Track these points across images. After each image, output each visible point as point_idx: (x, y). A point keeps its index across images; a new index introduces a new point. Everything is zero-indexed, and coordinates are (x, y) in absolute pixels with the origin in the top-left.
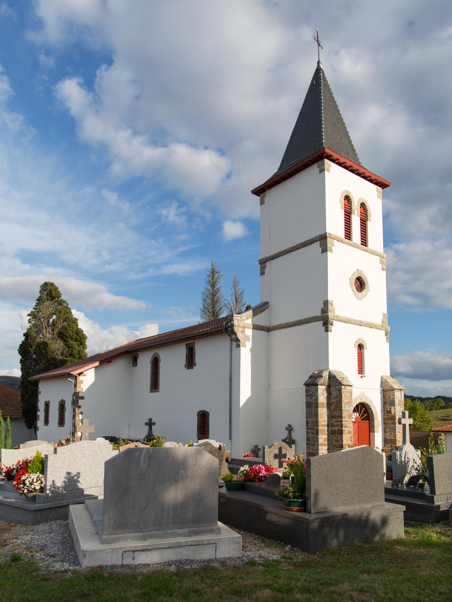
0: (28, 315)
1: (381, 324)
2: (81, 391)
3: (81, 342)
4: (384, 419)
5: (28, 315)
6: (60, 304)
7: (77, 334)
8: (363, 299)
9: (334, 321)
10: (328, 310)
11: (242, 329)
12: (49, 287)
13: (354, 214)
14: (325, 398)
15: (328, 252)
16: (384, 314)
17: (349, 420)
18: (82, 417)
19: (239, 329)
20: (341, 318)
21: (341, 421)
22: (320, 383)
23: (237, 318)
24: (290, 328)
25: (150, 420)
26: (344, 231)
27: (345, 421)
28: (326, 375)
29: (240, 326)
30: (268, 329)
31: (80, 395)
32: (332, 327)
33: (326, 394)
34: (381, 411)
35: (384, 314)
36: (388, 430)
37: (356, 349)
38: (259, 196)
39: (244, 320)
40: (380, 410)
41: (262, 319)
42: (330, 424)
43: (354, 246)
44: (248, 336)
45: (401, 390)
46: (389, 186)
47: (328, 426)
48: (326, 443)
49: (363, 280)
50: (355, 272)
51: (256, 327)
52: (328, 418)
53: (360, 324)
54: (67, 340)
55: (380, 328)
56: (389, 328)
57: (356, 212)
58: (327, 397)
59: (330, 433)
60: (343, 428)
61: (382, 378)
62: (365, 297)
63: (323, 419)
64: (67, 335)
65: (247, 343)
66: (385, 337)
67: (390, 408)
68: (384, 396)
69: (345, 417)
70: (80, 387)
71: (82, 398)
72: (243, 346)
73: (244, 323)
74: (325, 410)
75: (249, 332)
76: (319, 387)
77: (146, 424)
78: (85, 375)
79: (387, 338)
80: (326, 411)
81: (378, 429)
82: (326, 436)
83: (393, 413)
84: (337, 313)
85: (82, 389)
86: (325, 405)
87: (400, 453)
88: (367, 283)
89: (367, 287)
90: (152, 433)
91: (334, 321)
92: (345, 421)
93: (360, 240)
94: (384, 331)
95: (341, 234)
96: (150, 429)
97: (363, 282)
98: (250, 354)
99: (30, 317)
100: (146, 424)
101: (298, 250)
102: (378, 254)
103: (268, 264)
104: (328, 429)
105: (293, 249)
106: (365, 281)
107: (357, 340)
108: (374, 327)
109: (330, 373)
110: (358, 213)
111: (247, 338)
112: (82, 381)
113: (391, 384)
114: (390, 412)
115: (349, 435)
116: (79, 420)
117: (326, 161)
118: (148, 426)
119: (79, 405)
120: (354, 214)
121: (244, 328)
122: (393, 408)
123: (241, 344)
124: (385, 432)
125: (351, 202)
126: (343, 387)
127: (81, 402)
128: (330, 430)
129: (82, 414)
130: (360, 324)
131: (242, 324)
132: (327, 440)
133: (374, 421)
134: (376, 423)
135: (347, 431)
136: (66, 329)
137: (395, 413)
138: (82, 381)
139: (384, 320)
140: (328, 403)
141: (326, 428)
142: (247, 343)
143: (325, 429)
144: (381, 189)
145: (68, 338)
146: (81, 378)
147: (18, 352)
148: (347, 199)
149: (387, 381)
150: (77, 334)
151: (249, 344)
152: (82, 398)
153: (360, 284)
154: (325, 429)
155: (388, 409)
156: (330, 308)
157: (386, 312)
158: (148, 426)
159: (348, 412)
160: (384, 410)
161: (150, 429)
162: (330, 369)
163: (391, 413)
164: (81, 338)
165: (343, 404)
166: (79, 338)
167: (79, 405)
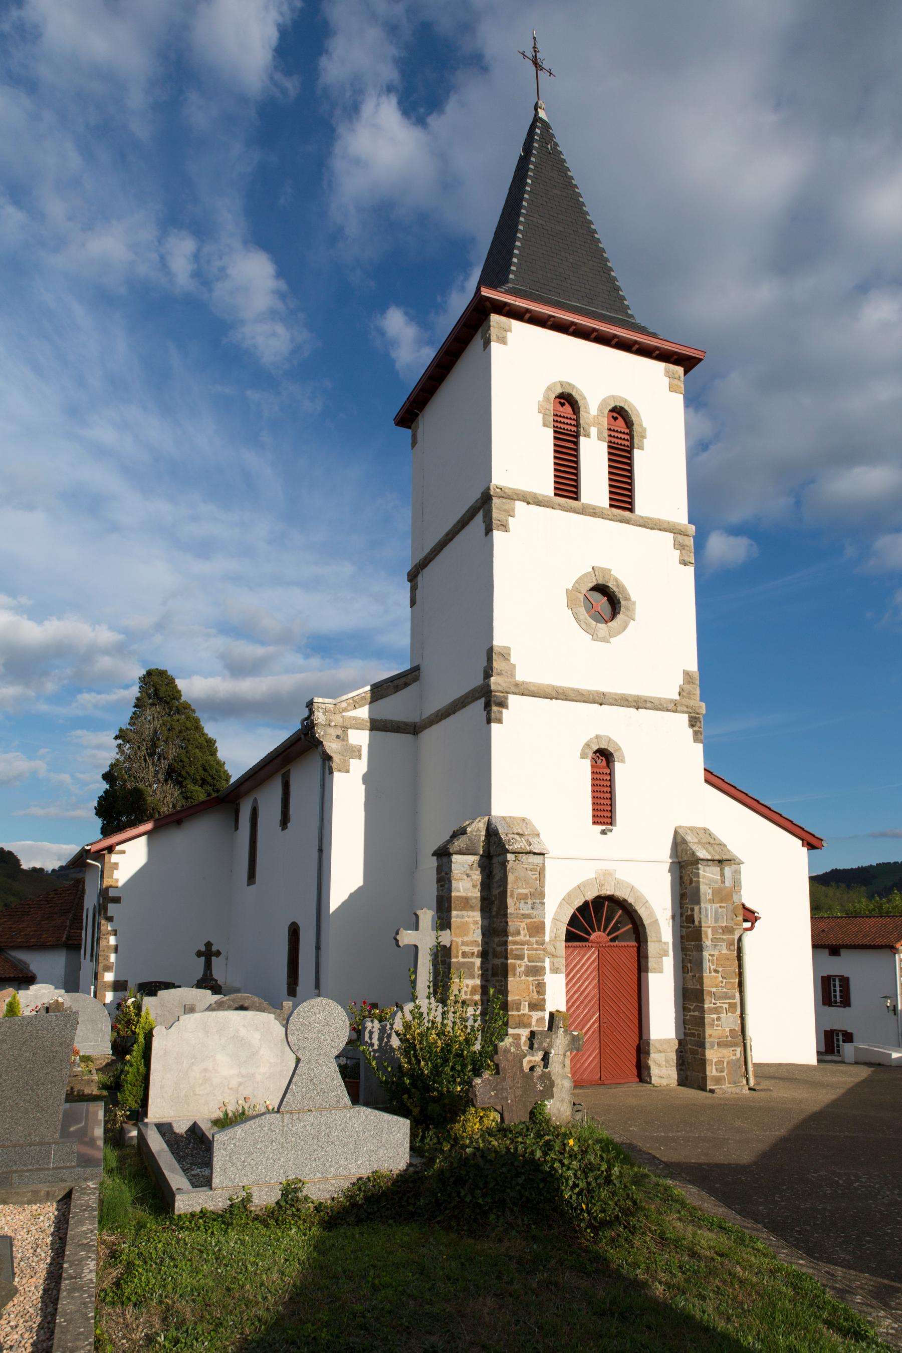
0: (116, 738)
1: (678, 698)
2: (114, 884)
3: (214, 785)
4: (682, 937)
5: (116, 738)
6: (178, 711)
7: (205, 770)
8: (612, 640)
9: (510, 697)
10: (492, 671)
11: (339, 732)
12: (155, 679)
13: (588, 435)
14: (474, 886)
15: (494, 531)
16: (687, 674)
17: (533, 940)
18: (117, 940)
19: (331, 731)
20: (533, 688)
21: (505, 943)
22: (457, 849)
23: (324, 706)
24: (443, 723)
25: (209, 945)
26: (607, 482)
27: (515, 943)
28: (478, 828)
29: (333, 724)
30: (414, 729)
31: (112, 893)
32: (504, 711)
33: (477, 876)
34: (673, 917)
35: (687, 674)
36: (689, 965)
37: (587, 763)
38: (409, 427)
39: (345, 710)
40: (669, 913)
41: (397, 707)
42: (491, 950)
43: (592, 512)
44: (355, 746)
45: (720, 861)
46: (700, 360)
47: (484, 955)
48: (477, 997)
49: (614, 592)
50: (585, 575)
51: (377, 726)
52: (483, 934)
53: (601, 699)
54: (184, 784)
55: (671, 706)
56: (703, 708)
57: (594, 431)
58: (482, 884)
59: (490, 972)
60: (509, 961)
61: (676, 832)
62: (620, 633)
63: (465, 939)
64: (183, 773)
65: (353, 762)
66: (691, 731)
67: (692, 910)
68: (681, 878)
69: (518, 933)
70: (111, 876)
71: (117, 900)
72: (339, 771)
73: (343, 717)
74: (476, 916)
75: (360, 738)
76: (455, 858)
77: (199, 954)
78: (123, 852)
79: (696, 733)
80: (479, 919)
81: (660, 964)
82: (478, 982)
83: (697, 923)
84: (520, 677)
85: (117, 880)
86: (478, 904)
87: (382, 1030)
88: (627, 599)
89: (627, 609)
90: (211, 975)
91: (510, 697)
92: (515, 943)
93: (607, 495)
94: (687, 716)
95: (545, 485)
96: (208, 966)
97: (616, 596)
98: (362, 788)
99: (120, 741)
100: (199, 954)
101: (458, 537)
102: (666, 526)
103: (420, 578)
104: (482, 963)
105: (450, 536)
106: (620, 596)
107: (591, 740)
108: (649, 705)
109: (489, 824)
110: (600, 432)
111: (356, 753)
112: (117, 864)
113: (694, 847)
114: (691, 919)
115: (531, 979)
116: (108, 947)
117: (495, 318)
118: (203, 959)
119: (109, 914)
120: (588, 435)
121: (345, 728)
122: (696, 908)
123: (334, 765)
124: (684, 972)
125: (579, 407)
126: (510, 857)
127: (112, 908)
128: (490, 966)
129: (115, 935)
130: (601, 699)
131: (337, 719)
132: (480, 991)
133: (647, 941)
134: (652, 948)
135: (523, 969)
136: (181, 761)
137: (700, 922)
138: (117, 864)
139: (687, 687)
140: (483, 899)
141: (478, 962)
142: (353, 762)
143: (473, 963)
144: (680, 370)
145: (185, 779)
146: (114, 858)
147: (94, 811)
148: (567, 400)
149: (684, 841)
150: (205, 770)
151: (359, 767)
152: (117, 900)
153: (606, 601)
154: (473, 963)
155: (689, 913)
156: (497, 664)
157: (693, 667)
158: (203, 959)
159: (528, 921)
160: (682, 915)
161: (208, 966)
162: (493, 813)
163: (693, 921)
164: (214, 779)
165: (510, 901)
166: (209, 779)
167: (109, 914)
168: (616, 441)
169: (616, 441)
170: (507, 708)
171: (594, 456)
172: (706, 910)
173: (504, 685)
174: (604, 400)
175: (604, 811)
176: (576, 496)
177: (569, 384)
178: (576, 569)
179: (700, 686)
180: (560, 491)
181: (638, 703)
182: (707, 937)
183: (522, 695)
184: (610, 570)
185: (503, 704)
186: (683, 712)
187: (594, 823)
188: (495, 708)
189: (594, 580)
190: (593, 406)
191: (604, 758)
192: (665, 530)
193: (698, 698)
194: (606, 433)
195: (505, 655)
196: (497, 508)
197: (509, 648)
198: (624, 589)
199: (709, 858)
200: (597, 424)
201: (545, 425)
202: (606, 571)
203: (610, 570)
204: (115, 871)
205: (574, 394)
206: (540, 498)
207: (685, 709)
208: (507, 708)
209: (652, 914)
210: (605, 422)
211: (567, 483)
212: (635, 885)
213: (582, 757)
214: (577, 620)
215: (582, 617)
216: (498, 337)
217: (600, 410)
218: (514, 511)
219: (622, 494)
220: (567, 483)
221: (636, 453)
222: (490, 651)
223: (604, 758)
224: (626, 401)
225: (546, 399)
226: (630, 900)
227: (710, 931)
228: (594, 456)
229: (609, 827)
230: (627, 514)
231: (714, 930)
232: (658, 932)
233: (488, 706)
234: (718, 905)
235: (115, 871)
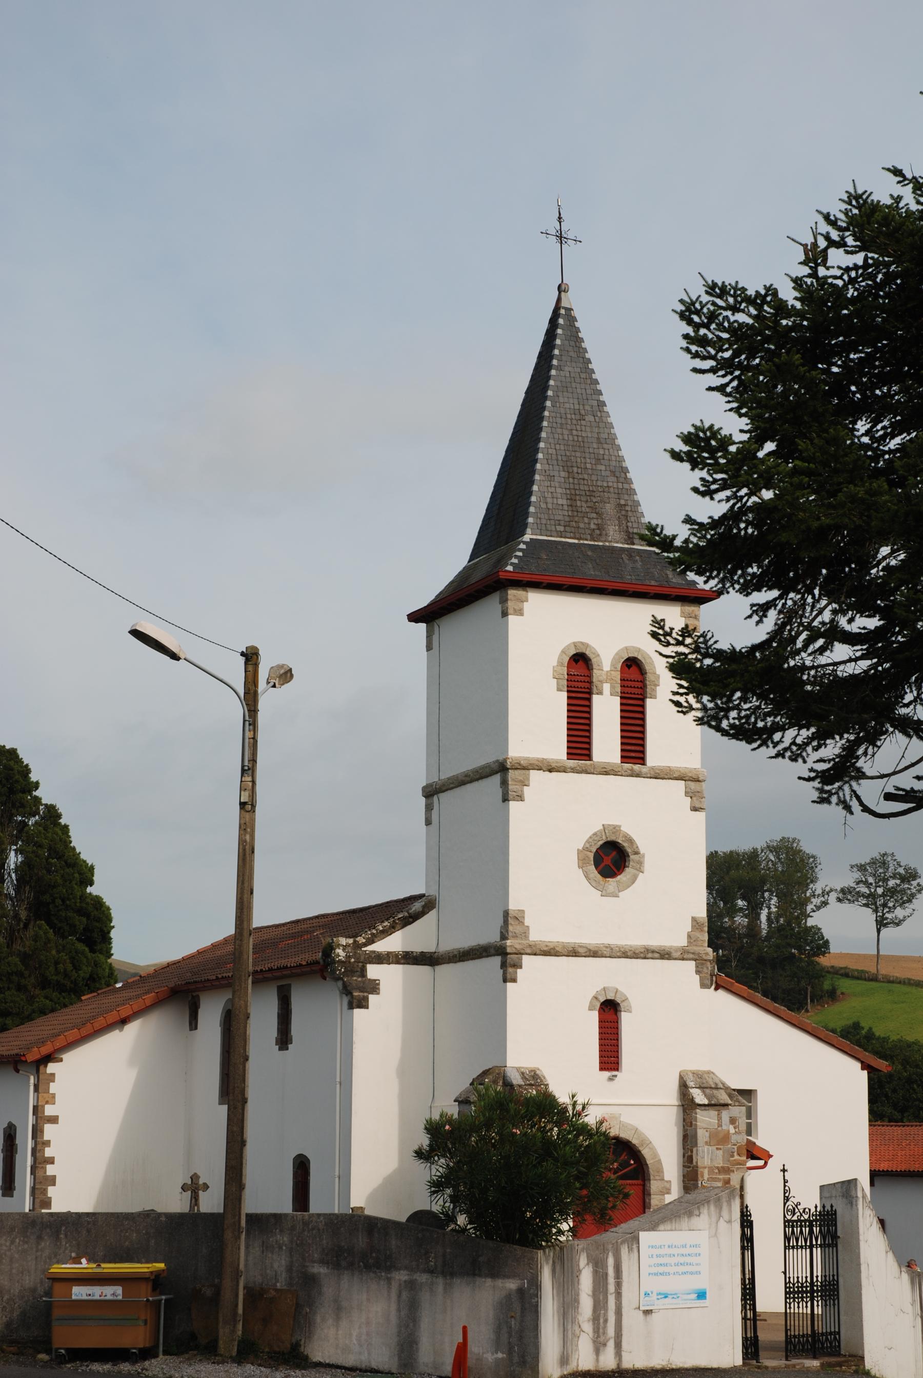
8: (621, 894)
13: (600, 693)
32: (519, 970)
37: (595, 1015)
43: (606, 771)
57: (606, 688)
95: (558, 750)
110: (612, 687)
122: (694, 1149)
153: (612, 858)
168: (576, 684)
169: (576, 684)
170: (521, 967)
171: (606, 711)
172: (703, 1152)
173: (518, 946)
174: (617, 654)
175: (610, 1058)
176: (642, 760)
177: (582, 643)
178: (585, 829)
179: (708, 932)
180: (626, 757)
181: (646, 953)
182: (702, 1176)
183: (535, 954)
184: (620, 826)
185: (518, 965)
186: (690, 959)
187: (601, 1069)
188: (510, 970)
189: (604, 837)
190: (606, 663)
191: (610, 1010)
192: (676, 779)
193: (706, 944)
194: (619, 689)
195: (519, 918)
196: (513, 780)
197: (523, 911)
198: (631, 841)
199: (706, 1102)
200: (609, 680)
201: (559, 690)
202: (616, 829)
203: (620, 826)
204: (46, 1149)
205: (587, 653)
206: (554, 765)
207: (691, 956)
208: (521, 967)
209: (655, 1155)
210: (617, 676)
211: (579, 742)
212: (640, 1128)
213: (590, 1010)
214: (587, 877)
215: (591, 876)
216: (515, 610)
217: (613, 665)
218: (528, 779)
219: (634, 746)
220: (579, 742)
221: (649, 702)
222: (506, 914)
223: (610, 1010)
224: (639, 650)
225: (560, 664)
226: (634, 1141)
227: (706, 1171)
228: (606, 711)
229: (615, 1073)
230: (637, 767)
231: (711, 1170)
232: (660, 1171)
233: (504, 965)
234: (714, 1148)
235: (46, 1149)
